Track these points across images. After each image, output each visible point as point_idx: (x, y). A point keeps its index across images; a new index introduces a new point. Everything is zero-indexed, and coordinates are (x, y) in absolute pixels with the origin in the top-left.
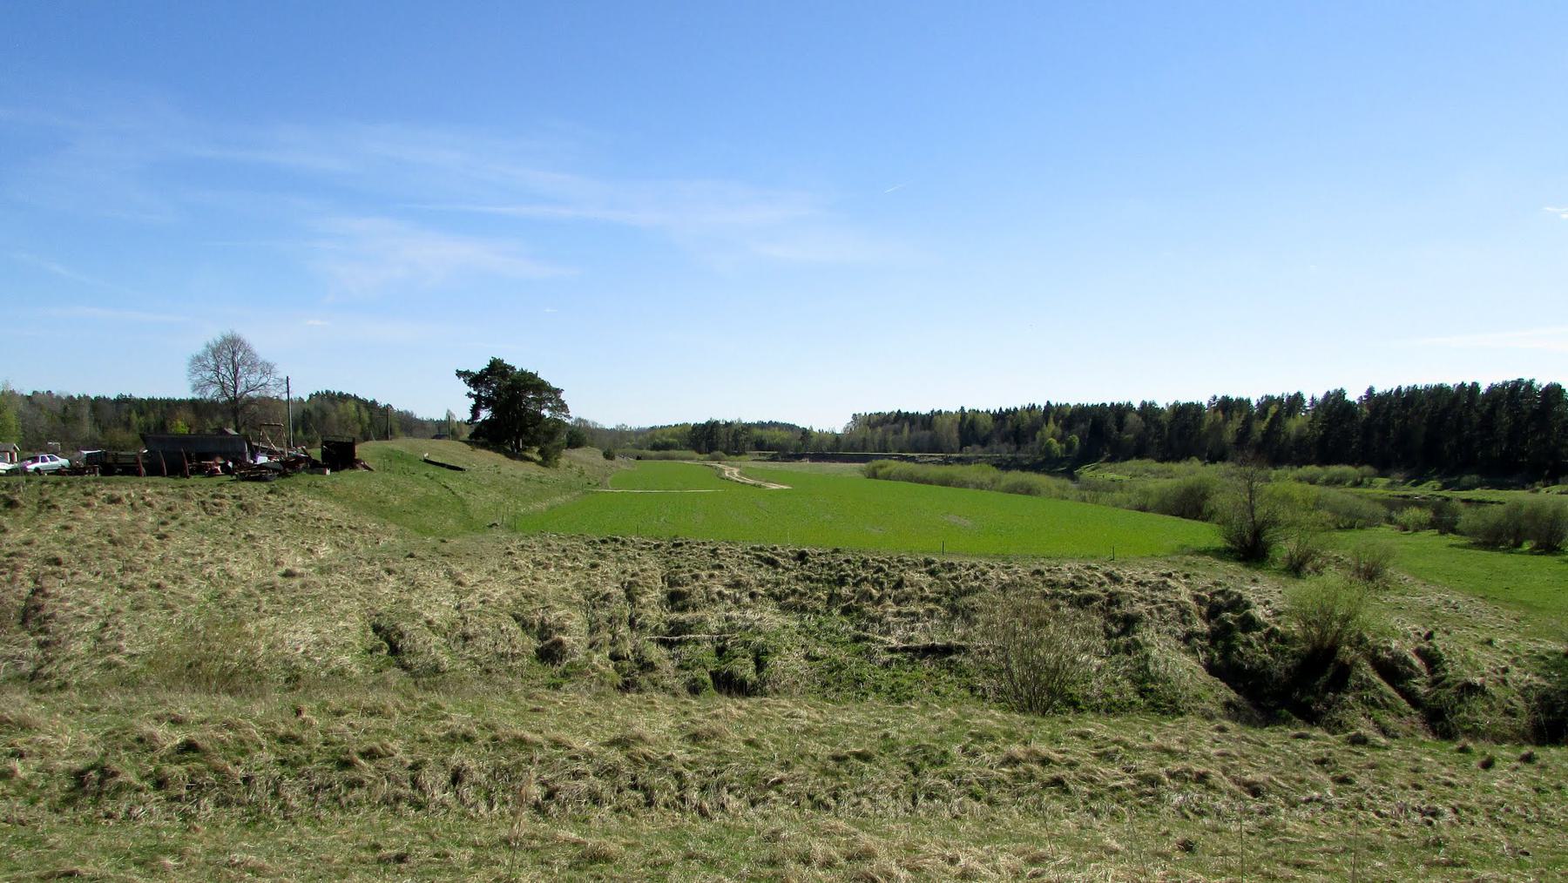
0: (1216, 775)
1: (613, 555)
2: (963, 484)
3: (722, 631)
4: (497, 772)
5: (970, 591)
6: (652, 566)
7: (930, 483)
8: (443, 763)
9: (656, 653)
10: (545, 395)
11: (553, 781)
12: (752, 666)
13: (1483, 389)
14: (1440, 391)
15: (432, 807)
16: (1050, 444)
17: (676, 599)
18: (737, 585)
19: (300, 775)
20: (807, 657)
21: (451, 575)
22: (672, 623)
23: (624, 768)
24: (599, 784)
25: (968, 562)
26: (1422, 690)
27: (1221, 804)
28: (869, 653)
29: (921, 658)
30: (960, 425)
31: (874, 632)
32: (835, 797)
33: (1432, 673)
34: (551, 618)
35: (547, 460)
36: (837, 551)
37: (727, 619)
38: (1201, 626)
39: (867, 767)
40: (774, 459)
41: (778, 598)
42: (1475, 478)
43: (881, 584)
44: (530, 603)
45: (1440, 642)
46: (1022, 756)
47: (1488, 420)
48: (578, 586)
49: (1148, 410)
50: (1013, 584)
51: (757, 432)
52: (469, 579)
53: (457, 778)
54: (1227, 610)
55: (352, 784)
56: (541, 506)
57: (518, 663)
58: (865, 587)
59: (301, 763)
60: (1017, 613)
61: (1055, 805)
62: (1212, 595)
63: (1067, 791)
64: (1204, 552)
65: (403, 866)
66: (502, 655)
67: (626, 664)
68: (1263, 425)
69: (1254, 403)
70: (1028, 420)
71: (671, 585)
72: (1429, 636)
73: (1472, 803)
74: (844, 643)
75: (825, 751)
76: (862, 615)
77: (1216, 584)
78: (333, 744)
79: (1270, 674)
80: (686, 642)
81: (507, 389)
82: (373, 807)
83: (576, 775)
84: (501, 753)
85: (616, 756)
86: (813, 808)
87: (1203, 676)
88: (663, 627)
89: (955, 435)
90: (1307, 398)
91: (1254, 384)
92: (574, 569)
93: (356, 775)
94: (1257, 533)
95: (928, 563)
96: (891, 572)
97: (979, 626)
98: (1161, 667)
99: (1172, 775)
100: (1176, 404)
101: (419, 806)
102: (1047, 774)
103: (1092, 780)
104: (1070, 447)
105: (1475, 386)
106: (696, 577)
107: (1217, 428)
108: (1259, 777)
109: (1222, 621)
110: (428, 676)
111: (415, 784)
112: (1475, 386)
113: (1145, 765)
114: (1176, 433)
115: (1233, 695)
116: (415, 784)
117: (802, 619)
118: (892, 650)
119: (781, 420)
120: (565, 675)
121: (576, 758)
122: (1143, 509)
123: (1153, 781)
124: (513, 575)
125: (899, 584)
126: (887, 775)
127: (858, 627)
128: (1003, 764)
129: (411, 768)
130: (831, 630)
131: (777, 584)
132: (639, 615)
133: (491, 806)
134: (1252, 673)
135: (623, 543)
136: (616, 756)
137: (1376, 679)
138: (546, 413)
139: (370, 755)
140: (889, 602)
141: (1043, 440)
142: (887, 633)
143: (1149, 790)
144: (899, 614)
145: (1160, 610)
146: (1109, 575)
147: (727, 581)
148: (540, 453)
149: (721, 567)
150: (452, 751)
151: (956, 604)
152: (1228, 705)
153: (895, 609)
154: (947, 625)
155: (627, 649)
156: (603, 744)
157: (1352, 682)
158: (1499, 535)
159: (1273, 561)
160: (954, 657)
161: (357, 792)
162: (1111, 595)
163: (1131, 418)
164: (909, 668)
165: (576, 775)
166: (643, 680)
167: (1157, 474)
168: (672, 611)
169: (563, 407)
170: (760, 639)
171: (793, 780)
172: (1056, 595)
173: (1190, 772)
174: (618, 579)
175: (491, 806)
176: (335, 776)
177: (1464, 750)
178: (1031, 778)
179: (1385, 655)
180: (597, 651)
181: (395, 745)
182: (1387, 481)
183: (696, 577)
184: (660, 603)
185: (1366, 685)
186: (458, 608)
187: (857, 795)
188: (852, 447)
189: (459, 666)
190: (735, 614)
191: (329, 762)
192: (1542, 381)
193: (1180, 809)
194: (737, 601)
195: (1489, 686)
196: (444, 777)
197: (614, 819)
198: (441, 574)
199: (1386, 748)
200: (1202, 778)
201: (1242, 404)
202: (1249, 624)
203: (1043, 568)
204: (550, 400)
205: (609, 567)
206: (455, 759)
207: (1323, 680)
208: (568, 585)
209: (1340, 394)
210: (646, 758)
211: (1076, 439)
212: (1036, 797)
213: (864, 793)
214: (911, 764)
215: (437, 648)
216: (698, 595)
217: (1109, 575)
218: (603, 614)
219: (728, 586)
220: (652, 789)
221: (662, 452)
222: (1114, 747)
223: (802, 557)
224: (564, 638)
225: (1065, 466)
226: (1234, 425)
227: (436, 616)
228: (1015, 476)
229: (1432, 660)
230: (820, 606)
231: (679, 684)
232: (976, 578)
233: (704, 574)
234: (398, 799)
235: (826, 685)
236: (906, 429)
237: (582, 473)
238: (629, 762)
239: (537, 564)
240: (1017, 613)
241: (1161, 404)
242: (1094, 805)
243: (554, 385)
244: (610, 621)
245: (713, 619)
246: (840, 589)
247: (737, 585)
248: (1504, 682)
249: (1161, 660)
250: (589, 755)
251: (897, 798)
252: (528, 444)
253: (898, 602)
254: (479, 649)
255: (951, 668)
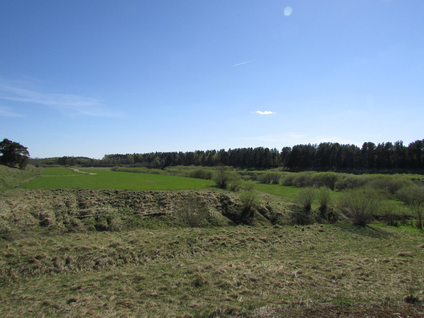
0: (256, 238)
1: (60, 194)
2: (140, 172)
3: (96, 213)
4: (80, 259)
5: (163, 199)
6: (73, 197)
7: (131, 172)
8: (62, 258)
9: (77, 221)
10: (22, 149)
11: (97, 259)
12: (107, 223)
13: (253, 149)
14: (245, 149)
15: (62, 272)
16: (157, 162)
17: (81, 205)
18: (99, 200)
19: (17, 267)
20: (122, 219)
21: (7, 202)
22: (81, 212)
23: (116, 253)
24: (110, 259)
25: (161, 192)
26: (269, 216)
27: (259, 245)
28: (139, 217)
29: (153, 217)
30: (134, 157)
31: (139, 211)
32: (174, 254)
33: (270, 211)
34: (43, 213)
35: (21, 168)
36: (126, 190)
37: (97, 210)
38: (219, 204)
39: (179, 245)
40: (83, 167)
41: (111, 204)
42: (254, 168)
43: (139, 198)
44: (36, 209)
45: (270, 204)
46: (213, 238)
47: (255, 155)
48: (50, 203)
49: (181, 153)
50: (174, 197)
51: (78, 159)
52: (15, 203)
53: (68, 261)
54: (225, 200)
55: (35, 268)
56: (27, 181)
57: (34, 227)
58: (135, 199)
59: (16, 263)
60: (176, 204)
61: (224, 250)
62: (221, 197)
63: (226, 246)
64: (213, 187)
65: (81, 290)
66: (29, 225)
67: (69, 225)
68: (208, 157)
69: (205, 152)
70: (151, 156)
71: (79, 201)
72: (268, 203)
73: (306, 239)
74: (132, 215)
75: (167, 243)
76: (135, 207)
77: (221, 194)
78: (24, 256)
79: (237, 215)
80: (86, 217)
81: (9, 147)
82: (43, 274)
83: (104, 257)
84: (79, 253)
85: (113, 250)
86: (169, 258)
87: (222, 216)
88: (78, 213)
89: (133, 160)
90: (216, 151)
91: (205, 147)
92: (48, 198)
93: (36, 265)
94: (223, 182)
95: (151, 192)
96: (142, 195)
97: (167, 208)
98: (213, 215)
99: (247, 240)
100: (187, 152)
101: (58, 272)
102: (222, 242)
103: (231, 243)
104: (162, 162)
105: (252, 148)
106: (87, 199)
107: (197, 158)
108: (265, 238)
109: (224, 203)
110: (4, 233)
111: (55, 265)
112: (252, 148)
113: (240, 237)
114: (188, 159)
115: (230, 220)
116: (55, 265)
117: (119, 209)
118: (145, 215)
119: (84, 156)
120: (50, 229)
121: (102, 252)
122: (187, 177)
123: (244, 241)
124: (28, 201)
125: (144, 198)
126: (184, 247)
127: (135, 210)
128: (209, 241)
129: (52, 260)
130: (127, 211)
131: (111, 200)
132: (71, 211)
133: (80, 269)
134: (233, 215)
135: (63, 190)
136: (113, 250)
137: (259, 214)
138: (22, 154)
139: (38, 258)
140: (142, 203)
141: (155, 161)
142: (143, 211)
143: (243, 243)
144: (145, 206)
145: (210, 201)
146: (196, 193)
147: (96, 199)
148: (19, 166)
149: (93, 196)
150: (64, 254)
151: (161, 203)
152: (229, 222)
153: (144, 205)
154: (158, 207)
155: (68, 220)
156: (108, 247)
157: (254, 215)
158: (269, 180)
159: (227, 188)
160: (162, 216)
161: (37, 270)
162: (198, 198)
163: (177, 156)
164: (150, 220)
165: (104, 257)
166: (74, 229)
167: (184, 169)
168: (81, 209)
169: (27, 153)
170: (108, 215)
171: (161, 251)
172: (185, 199)
173: (250, 238)
174: (63, 201)
175: (80, 269)
176: (29, 266)
177: (296, 227)
178: (217, 244)
179: (260, 208)
180: (59, 222)
181: (45, 254)
182: (236, 169)
183: (87, 199)
184: (77, 207)
185: (257, 215)
186: (12, 212)
187: (179, 253)
188: (105, 163)
189: (14, 229)
190: (99, 208)
191: (25, 262)
192: (265, 147)
193: (251, 247)
194: (99, 205)
195: (282, 213)
196: (63, 262)
197: (117, 268)
198: (4, 202)
199: (283, 228)
200: (253, 239)
201: (202, 152)
202: (230, 203)
203: (180, 192)
204: (23, 151)
205: (59, 197)
206: (66, 256)
207: (249, 215)
208: (47, 203)
209: (224, 150)
210: (122, 249)
211: (164, 161)
212: (220, 248)
213: (180, 252)
214: (188, 244)
215: (7, 224)
216: (88, 204)
217: (196, 193)
218: (59, 211)
219: (96, 201)
220: (126, 259)
221: (50, 165)
222: (231, 234)
223: (116, 192)
224: (49, 219)
225: (163, 167)
226: (201, 157)
227: (5, 215)
228: (153, 170)
229: (269, 208)
230: (123, 205)
231: (85, 229)
232: (164, 195)
233: (89, 198)
234: (51, 270)
235: (128, 226)
236: (120, 159)
237: (32, 171)
238: (117, 251)
239: (36, 197)
240: (176, 204)
241: (184, 152)
242: (233, 249)
243: (25, 146)
244: (62, 213)
245: (93, 210)
246: (129, 200)
247: (99, 200)
248: (285, 212)
249: (212, 213)
250: (105, 251)
251: (188, 253)
252: (15, 163)
253: (145, 203)
254: (21, 224)
255: (161, 219)
